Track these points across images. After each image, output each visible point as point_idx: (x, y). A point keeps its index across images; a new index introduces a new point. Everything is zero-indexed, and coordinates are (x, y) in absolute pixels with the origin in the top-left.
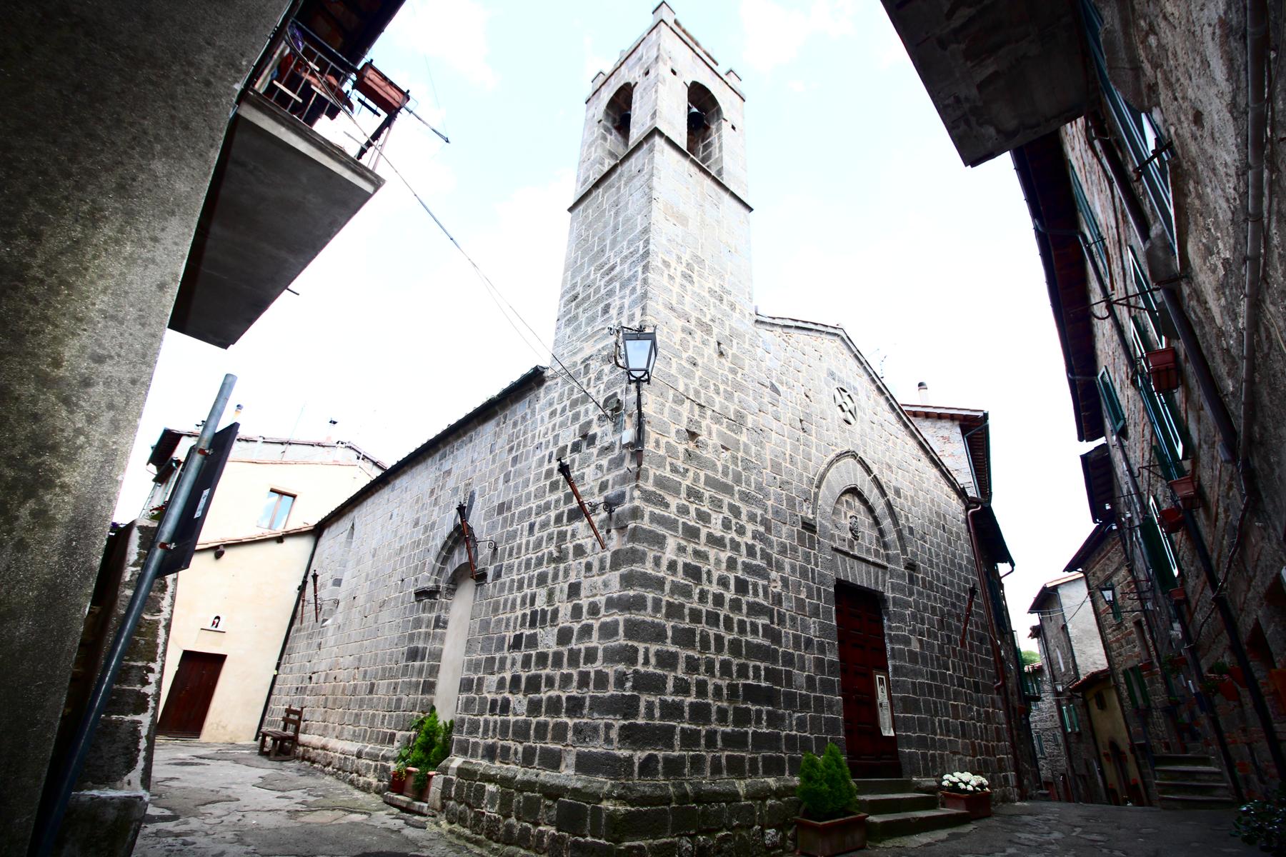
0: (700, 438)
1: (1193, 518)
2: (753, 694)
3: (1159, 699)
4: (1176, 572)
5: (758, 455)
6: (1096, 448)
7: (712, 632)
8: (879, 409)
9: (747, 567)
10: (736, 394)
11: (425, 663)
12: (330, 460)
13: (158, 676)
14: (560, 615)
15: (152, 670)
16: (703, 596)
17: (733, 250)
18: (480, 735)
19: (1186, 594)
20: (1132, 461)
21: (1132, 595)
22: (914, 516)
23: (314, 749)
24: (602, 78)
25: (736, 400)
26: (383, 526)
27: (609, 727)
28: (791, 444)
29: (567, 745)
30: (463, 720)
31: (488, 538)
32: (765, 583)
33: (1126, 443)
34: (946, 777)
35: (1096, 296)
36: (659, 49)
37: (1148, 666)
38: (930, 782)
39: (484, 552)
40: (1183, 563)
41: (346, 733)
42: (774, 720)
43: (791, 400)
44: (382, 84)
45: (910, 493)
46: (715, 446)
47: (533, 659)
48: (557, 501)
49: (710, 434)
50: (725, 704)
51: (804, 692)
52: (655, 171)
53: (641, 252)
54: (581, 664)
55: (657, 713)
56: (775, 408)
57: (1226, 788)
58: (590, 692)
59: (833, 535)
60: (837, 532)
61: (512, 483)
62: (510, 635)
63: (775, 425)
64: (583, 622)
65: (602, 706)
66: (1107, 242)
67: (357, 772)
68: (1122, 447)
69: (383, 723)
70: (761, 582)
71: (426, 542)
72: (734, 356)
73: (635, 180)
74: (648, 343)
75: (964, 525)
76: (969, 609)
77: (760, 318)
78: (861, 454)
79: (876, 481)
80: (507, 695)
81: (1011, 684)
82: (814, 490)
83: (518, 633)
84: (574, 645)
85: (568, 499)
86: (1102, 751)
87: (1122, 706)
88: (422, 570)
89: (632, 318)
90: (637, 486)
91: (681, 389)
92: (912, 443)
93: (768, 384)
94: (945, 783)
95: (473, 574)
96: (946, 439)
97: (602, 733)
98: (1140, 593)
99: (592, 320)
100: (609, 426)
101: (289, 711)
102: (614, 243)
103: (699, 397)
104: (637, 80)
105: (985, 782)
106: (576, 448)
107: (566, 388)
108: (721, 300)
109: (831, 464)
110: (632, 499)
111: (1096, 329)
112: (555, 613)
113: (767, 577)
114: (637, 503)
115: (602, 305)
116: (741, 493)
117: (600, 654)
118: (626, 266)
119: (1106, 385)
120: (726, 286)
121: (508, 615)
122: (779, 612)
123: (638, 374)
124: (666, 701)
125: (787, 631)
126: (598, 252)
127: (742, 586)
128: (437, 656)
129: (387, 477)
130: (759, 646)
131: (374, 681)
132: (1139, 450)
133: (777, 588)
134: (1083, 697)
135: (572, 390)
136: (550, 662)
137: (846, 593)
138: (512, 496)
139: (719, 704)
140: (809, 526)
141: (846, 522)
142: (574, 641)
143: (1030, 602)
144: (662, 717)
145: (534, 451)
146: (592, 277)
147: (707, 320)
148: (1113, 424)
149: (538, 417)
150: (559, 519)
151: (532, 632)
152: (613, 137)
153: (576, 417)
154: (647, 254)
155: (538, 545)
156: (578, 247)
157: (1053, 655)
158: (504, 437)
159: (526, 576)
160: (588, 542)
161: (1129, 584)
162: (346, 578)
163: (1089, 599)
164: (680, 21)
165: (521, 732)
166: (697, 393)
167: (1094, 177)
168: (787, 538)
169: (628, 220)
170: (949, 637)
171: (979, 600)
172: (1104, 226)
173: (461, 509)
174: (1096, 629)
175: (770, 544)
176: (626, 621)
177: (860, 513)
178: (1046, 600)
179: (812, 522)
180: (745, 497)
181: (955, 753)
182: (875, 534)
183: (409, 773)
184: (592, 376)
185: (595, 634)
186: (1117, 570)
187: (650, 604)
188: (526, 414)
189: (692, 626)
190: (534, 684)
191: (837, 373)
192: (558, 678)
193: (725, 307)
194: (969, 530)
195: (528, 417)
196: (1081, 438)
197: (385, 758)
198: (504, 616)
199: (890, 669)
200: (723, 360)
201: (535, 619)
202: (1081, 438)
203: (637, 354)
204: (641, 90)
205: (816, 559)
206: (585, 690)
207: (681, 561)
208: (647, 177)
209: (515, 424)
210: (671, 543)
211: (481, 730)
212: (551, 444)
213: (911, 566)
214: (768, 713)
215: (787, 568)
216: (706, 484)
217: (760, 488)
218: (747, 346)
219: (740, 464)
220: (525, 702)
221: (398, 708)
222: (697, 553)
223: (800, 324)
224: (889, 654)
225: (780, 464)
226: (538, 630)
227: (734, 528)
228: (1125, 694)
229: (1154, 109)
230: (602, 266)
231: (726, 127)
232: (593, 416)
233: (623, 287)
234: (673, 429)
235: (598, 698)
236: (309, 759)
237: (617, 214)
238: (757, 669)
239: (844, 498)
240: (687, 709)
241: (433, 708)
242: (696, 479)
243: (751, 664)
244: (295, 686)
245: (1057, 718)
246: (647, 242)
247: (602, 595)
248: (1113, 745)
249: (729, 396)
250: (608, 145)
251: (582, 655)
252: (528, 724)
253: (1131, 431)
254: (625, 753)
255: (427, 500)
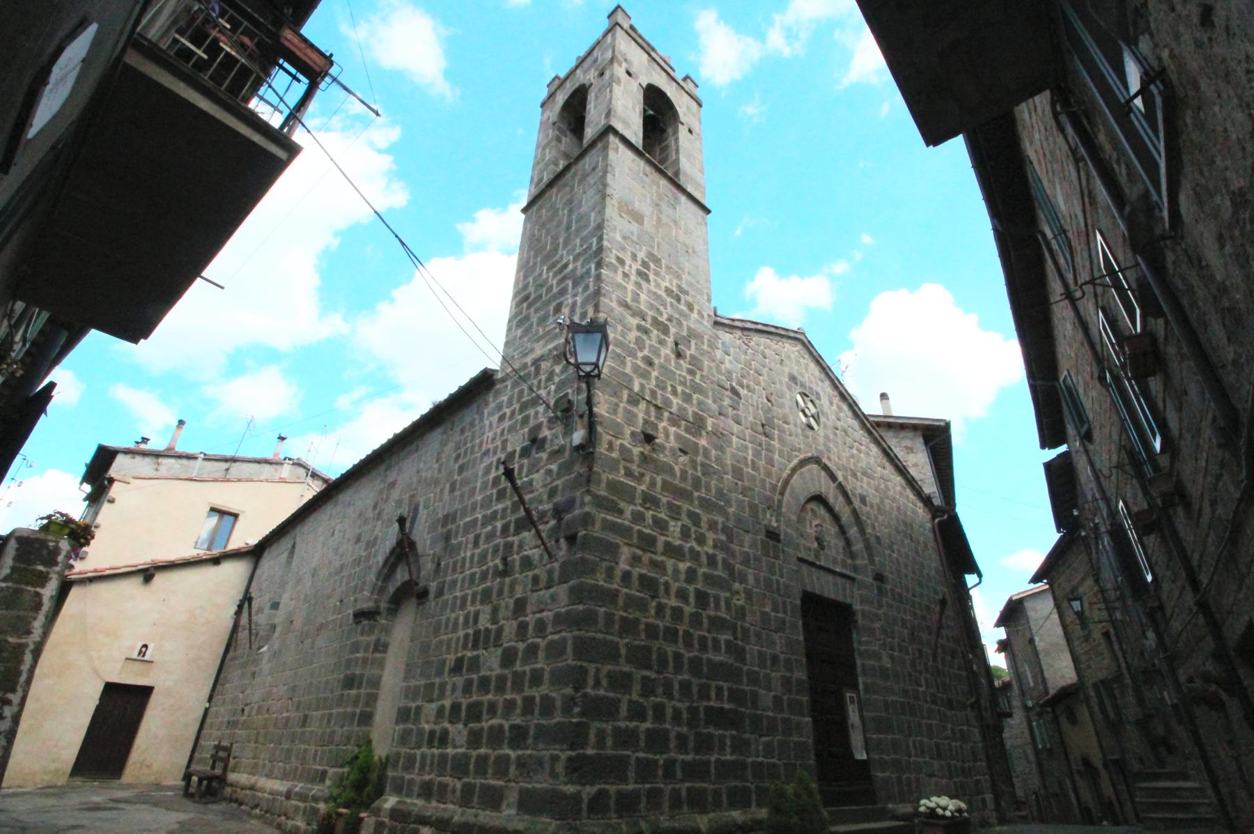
0: (657, 441)
1: (1170, 519)
2: (717, 717)
3: (1131, 711)
4: (1149, 578)
5: (718, 459)
6: (1059, 456)
7: (670, 649)
8: (842, 415)
9: (709, 579)
10: (695, 396)
11: (363, 691)
12: (277, 478)
13: (15, 709)
14: (504, 634)
15: (9, 702)
16: (660, 609)
17: (690, 251)
18: (417, 770)
19: (1159, 599)
20: (1098, 466)
21: (1099, 606)
22: (880, 527)
23: (242, 789)
24: (557, 82)
25: (695, 402)
26: (324, 544)
27: (555, 759)
28: (754, 450)
29: (509, 781)
30: (398, 754)
31: (432, 552)
32: (728, 595)
33: (1091, 447)
34: (923, 802)
35: (1056, 288)
36: (614, 51)
37: (1118, 677)
38: (907, 809)
39: (428, 566)
40: (1157, 569)
41: (276, 771)
42: (740, 746)
43: (753, 399)
44: (302, 45)
45: (876, 501)
46: (672, 449)
47: (475, 684)
48: (504, 510)
49: (667, 435)
50: (685, 730)
51: (770, 714)
52: (609, 168)
53: (594, 248)
54: (526, 689)
55: (609, 742)
56: (735, 412)
57: (1208, 805)
58: (536, 720)
59: (798, 545)
60: (802, 542)
61: (457, 493)
62: (451, 658)
63: (736, 428)
64: (529, 641)
65: (545, 735)
66: (1070, 235)
67: (285, 815)
68: (1087, 451)
69: (315, 758)
70: (724, 595)
71: (368, 558)
72: (692, 356)
73: (589, 179)
74: (598, 336)
75: (931, 535)
76: (940, 621)
77: (719, 319)
78: (825, 460)
79: (841, 487)
80: (446, 725)
81: (984, 702)
82: (777, 497)
83: (459, 655)
84: (518, 667)
85: (515, 508)
86: (1074, 767)
87: (1093, 720)
88: (362, 590)
89: (584, 315)
90: (588, 492)
91: (636, 388)
92: (874, 450)
93: (728, 386)
94: (922, 809)
95: (411, 593)
96: (910, 450)
97: (547, 766)
98: (1105, 601)
99: (543, 320)
100: (559, 429)
101: (218, 748)
102: (566, 243)
103: (656, 398)
104: (593, 81)
105: (963, 805)
106: (525, 452)
107: (516, 390)
108: (679, 300)
109: (794, 470)
110: (583, 504)
111: (1056, 332)
112: (500, 631)
113: (729, 589)
114: (587, 509)
115: (554, 304)
116: (700, 499)
117: (546, 676)
118: (579, 264)
119: (1069, 390)
120: (684, 286)
121: (450, 636)
122: (742, 627)
123: (588, 369)
124: (619, 727)
125: (752, 648)
126: (550, 251)
127: (702, 598)
128: (376, 683)
129: (332, 491)
130: (721, 664)
131: (307, 712)
132: (1105, 452)
133: (740, 601)
134: (1053, 711)
135: (522, 392)
136: (492, 687)
137: (813, 605)
138: (457, 506)
139: (679, 729)
140: (773, 535)
141: (811, 531)
142: (518, 663)
143: (997, 615)
144: (615, 746)
145: (482, 458)
146: (544, 276)
147: (663, 319)
148: (1077, 428)
149: (487, 422)
150: (505, 529)
151: (475, 653)
152: (568, 140)
153: (525, 420)
154: (600, 249)
155: (483, 557)
156: (530, 248)
157: (1021, 670)
158: (451, 445)
159: (470, 592)
160: (535, 553)
161: (1095, 595)
162: (285, 599)
163: (1055, 610)
164: (637, 26)
165: (460, 766)
166: (653, 393)
167: (1055, 166)
168: (750, 547)
169: (581, 218)
170: (920, 651)
171: (949, 612)
172: (1067, 216)
173: (401, 521)
174: (1063, 642)
175: (733, 555)
176: (575, 638)
177: (824, 521)
178: (1013, 613)
179: (776, 531)
180: (706, 504)
181: (931, 776)
182: (841, 543)
183: (340, 815)
184: (543, 377)
185: (541, 655)
186: (1083, 580)
187: (601, 620)
188: (474, 420)
189: (649, 643)
190: (475, 712)
191: (799, 377)
192: (500, 705)
193: (683, 307)
194: (936, 540)
195: (477, 422)
196: (1043, 446)
197: (316, 799)
198: (445, 637)
199: (861, 687)
200: (682, 362)
201: (479, 639)
202: (1043, 446)
203: (586, 355)
204: (596, 90)
205: (781, 569)
206: (529, 717)
207: (636, 571)
208: (601, 174)
209: (462, 431)
210: (625, 552)
211: (417, 765)
212: (499, 450)
213: (879, 578)
214: (733, 738)
215: (751, 580)
216: (663, 488)
217: (720, 494)
218: (705, 347)
219: (699, 468)
220: (465, 733)
221: (331, 742)
222: (654, 564)
223: (760, 327)
224: (859, 670)
225: (742, 469)
226: (481, 652)
227: (693, 536)
228: (1096, 708)
229: (1141, 38)
230: (554, 266)
231: (682, 132)
232: (542, 419)
233: (575, 285)
234: (628, 431)
235: (543, 726)
236: (236, 801)
237: (571, 211)
238: (719, 690)
239: (810, 506)
240: (642, 737)
241: (369, 742)
242: (653, 484)
243: (713, 684)
244: (226, 719)
245: (1027, 732)
246: (600, 239)
247: (549, 610)
248: (1086, 762)
249: (687, 398)
250: (562, 147)
251: (527, 678)
252: (467, 757)
253: (1096, 435)
254: (570, 789)
255: (370, 514)
